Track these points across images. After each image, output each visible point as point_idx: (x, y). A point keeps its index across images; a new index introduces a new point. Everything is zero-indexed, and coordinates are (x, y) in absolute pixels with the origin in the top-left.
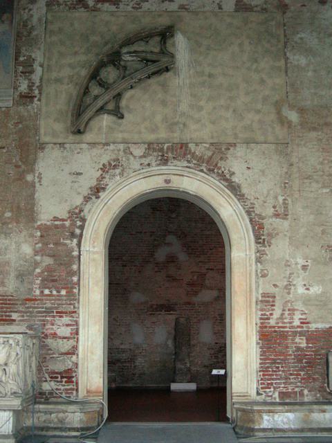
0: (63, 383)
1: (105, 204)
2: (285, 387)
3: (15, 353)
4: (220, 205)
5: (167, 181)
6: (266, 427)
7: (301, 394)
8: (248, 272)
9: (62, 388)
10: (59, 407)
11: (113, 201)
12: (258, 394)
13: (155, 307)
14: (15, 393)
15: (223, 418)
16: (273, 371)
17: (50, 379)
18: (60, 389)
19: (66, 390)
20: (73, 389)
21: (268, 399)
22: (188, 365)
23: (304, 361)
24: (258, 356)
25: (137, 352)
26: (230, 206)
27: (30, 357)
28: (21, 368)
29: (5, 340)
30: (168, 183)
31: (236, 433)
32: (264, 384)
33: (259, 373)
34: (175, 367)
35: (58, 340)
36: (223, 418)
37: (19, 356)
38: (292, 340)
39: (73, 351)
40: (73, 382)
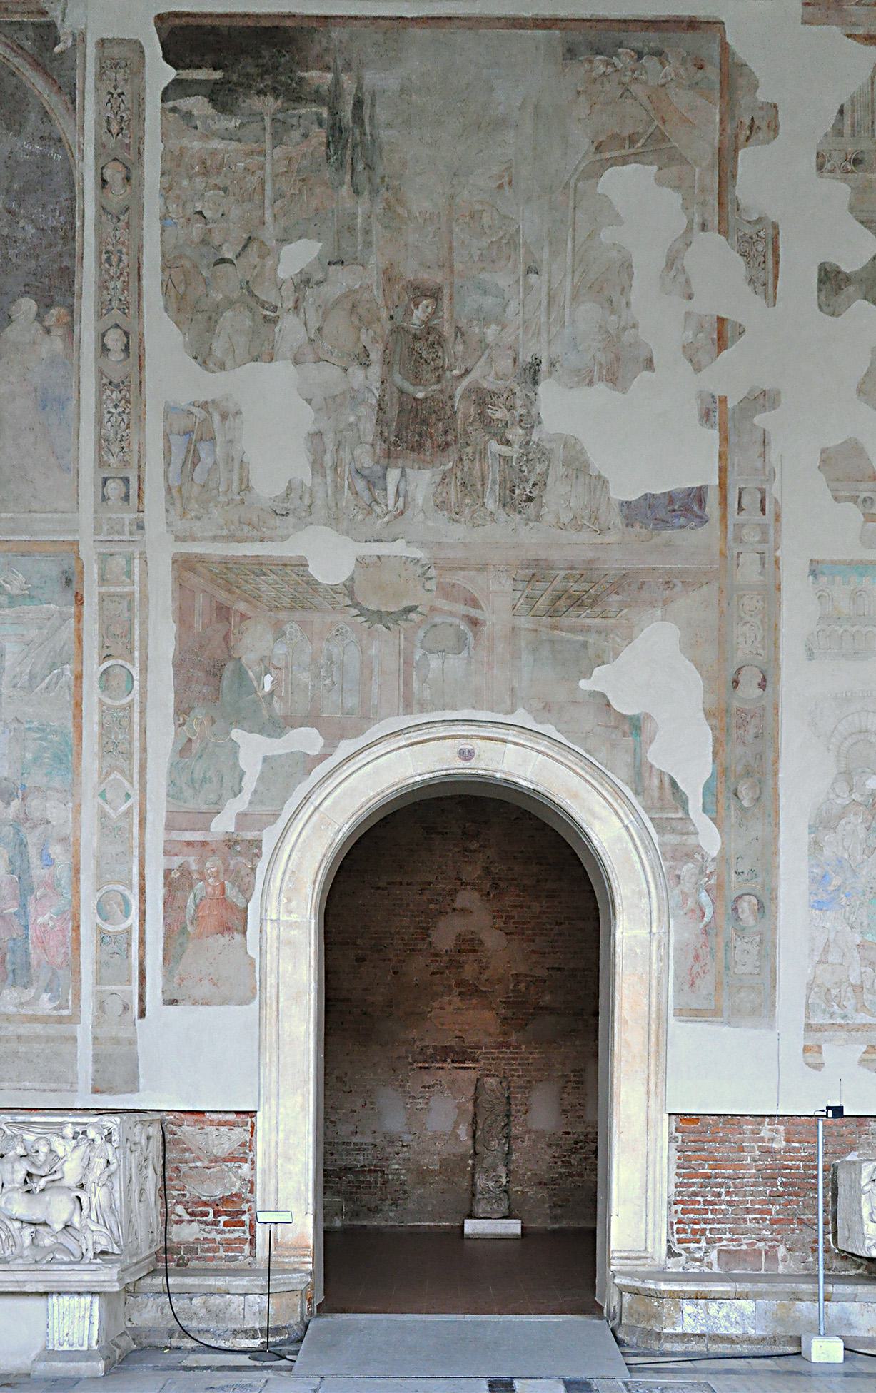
0: (221, 1227)
1: (316, 808)
2: (732, 1240)
3: (103, 1161)
4: (594, 815)
5: (466, 755)
6: (689, 1331)
7: (771, 1256)
8: (655, 974)
9: (218, 1237)
10: (211, 1281)
11: (335, 803)
12: (671, 1253)
13: (430, 1051)
14: (103, 1253)
15: (592, 1308)
16: (706, 1203)
17: (187, 1217)
18: (214, 1241)
19: (229, 1241)
20: (244, 1241)
21: (694, 1268)
22: (504, 1181)
23: (779, 1181)
24: (674, 1170)
25: (389, 1150)
26: (614, 818)
27: (141, 1168)
28: (117, 1195)
29: (79, 1129)
30: (466, 759)
31: (620, 1342)
32: (684, 1231)
33: (674, 1208)
34: (473, 1185)
35: (208, 1129)
36: (592, 1308)
37: (113, 1167)
38: (753, 1132)
39: (245, 1153)
40: (243, 1224)
